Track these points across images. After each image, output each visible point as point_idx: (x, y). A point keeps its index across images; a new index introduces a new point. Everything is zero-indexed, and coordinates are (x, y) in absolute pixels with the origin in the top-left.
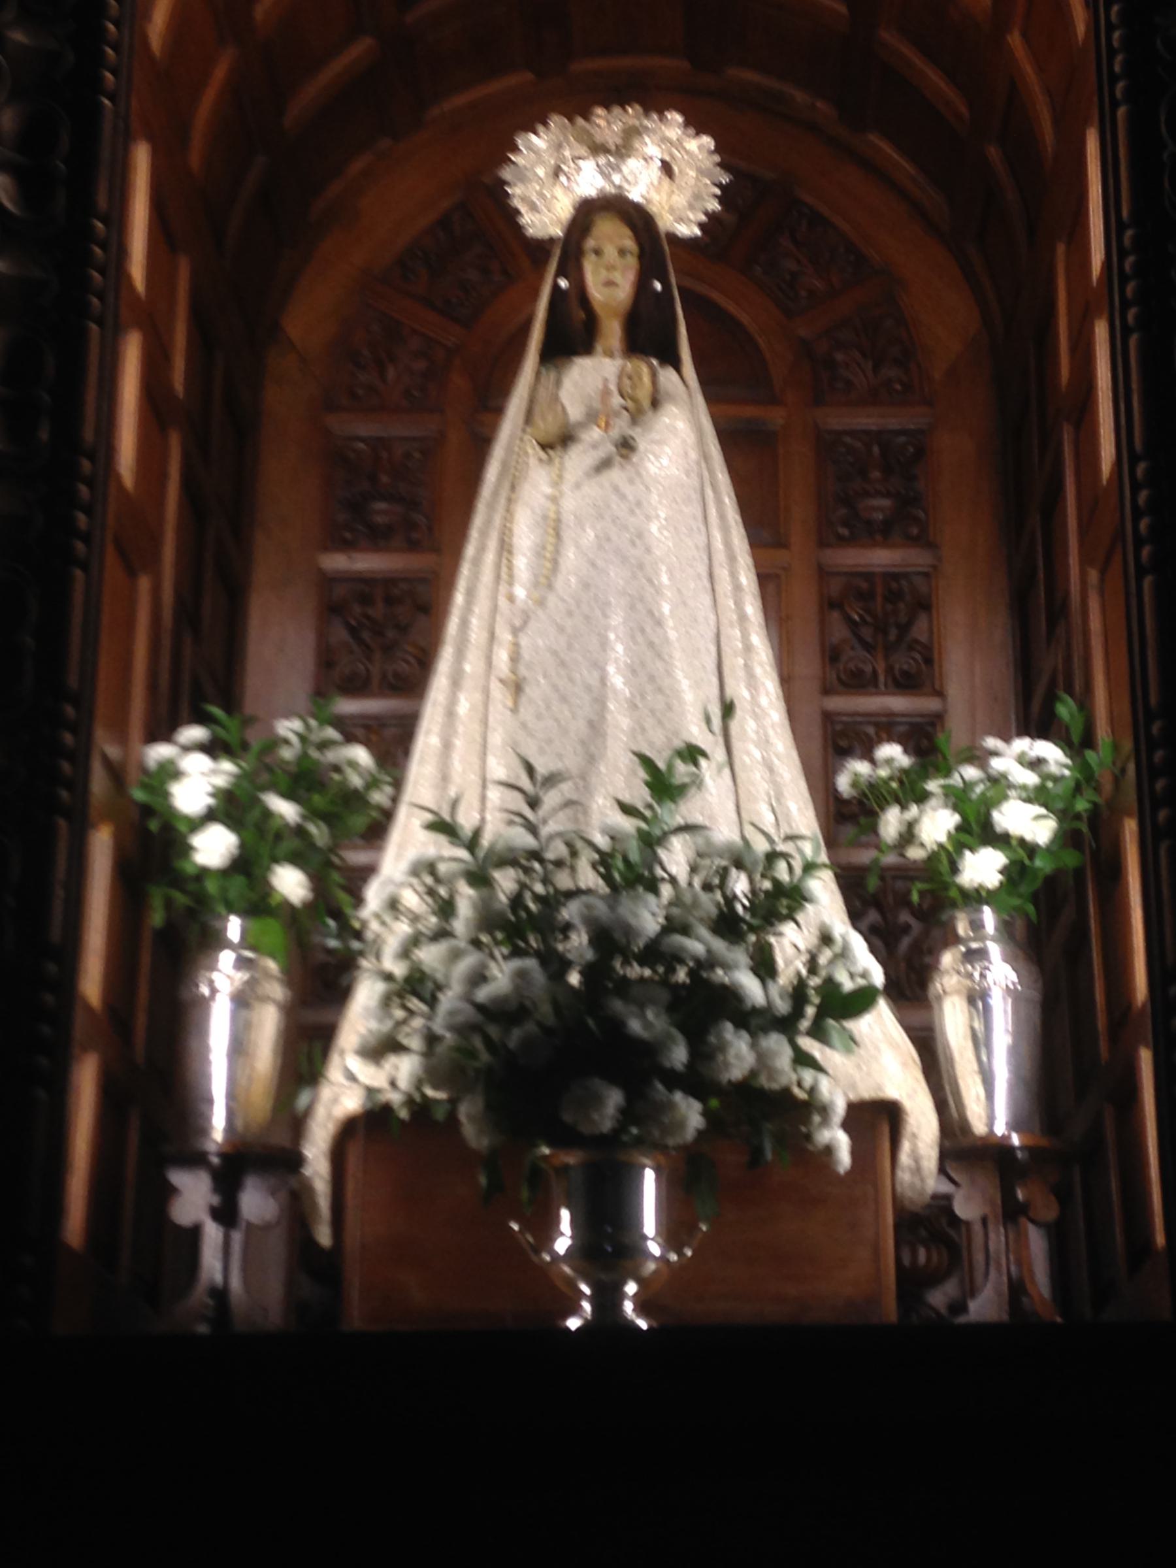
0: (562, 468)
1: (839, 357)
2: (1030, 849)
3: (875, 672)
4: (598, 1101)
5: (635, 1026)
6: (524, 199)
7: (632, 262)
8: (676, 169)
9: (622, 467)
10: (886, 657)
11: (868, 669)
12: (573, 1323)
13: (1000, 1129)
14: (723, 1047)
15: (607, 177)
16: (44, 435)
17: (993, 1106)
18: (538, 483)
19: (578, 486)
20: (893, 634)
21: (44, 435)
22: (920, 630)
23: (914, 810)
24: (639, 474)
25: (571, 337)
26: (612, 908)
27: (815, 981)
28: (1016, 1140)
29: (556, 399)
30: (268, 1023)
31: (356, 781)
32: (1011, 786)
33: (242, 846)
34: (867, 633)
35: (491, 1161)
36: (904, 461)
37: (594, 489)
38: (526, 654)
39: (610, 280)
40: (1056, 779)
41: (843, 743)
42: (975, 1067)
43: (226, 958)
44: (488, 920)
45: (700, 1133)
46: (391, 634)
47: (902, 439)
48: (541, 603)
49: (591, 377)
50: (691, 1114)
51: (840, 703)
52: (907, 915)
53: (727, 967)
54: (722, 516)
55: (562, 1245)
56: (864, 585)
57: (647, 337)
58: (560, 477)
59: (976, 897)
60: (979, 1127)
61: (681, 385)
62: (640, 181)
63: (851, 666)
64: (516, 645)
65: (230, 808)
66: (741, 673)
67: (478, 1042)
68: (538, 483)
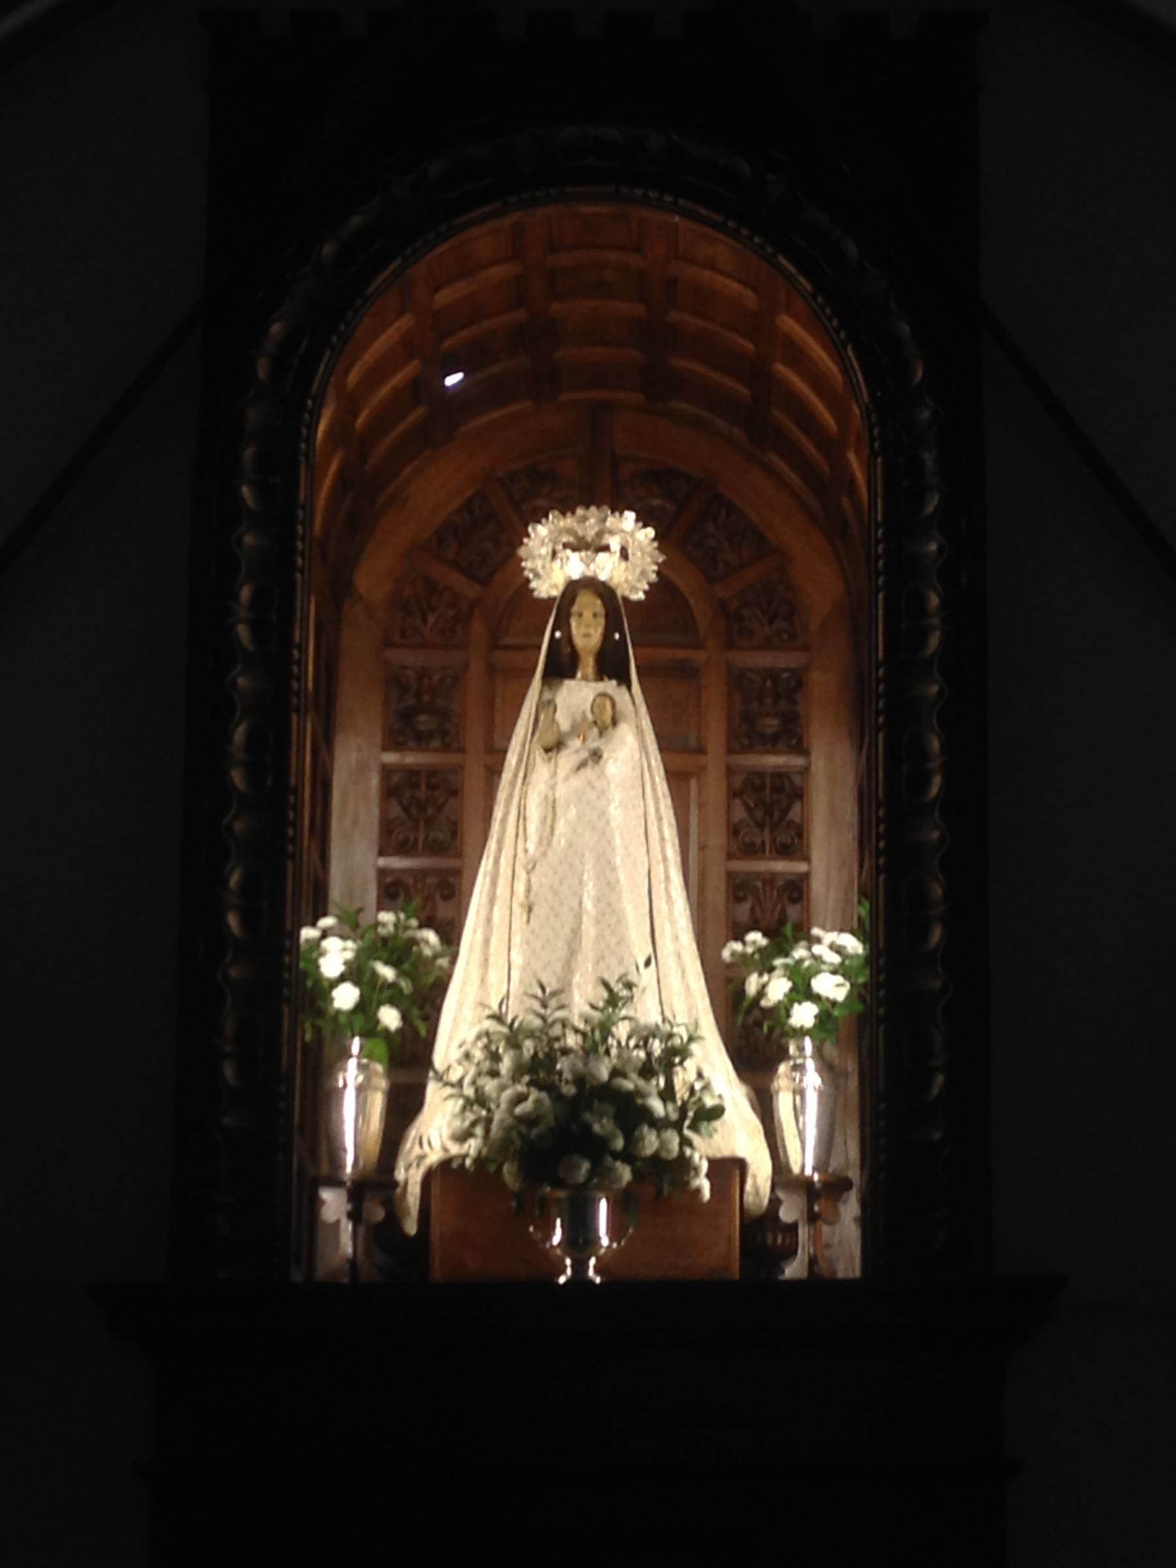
0: (556, 766)
1: (746, 613)
2: (834, 1003)
3: (763, 843)
4: (578, 1167)
5: (596, 1128)
6: (534, 571)
7: (602, 621)
8: (630, 552)
9: (593, 768)
10: (772, 831)
11: (759, 841)
12: (562, 1280)
13: (808, 1172)
14: (642, 1138)
15: (588, 565)
16: (269, 782)
17: (803, 1157)
18: (542, 772)
19: (566, 779)
20: (777, 814)
21: (269, 782)
22: (795, 813)
23: (766, 977)
24: (603, 772)
25: (562, 666)
26: (586, 1064)
27: (693, 1099)
28: (816, 1177)
29: (553, 720)
30: (377, 1102)
31: (427, 952)
32: (823, 962)
33: (362, 995)
34: (759, 814)
35: (519, 1195)
36: (788, 690)
37: (577, 782)
38: (535, 887)
39: (587, 632)
40: (851, 957)
41: (741, 894)
42: (796, 1132)
43: (352, 1064)
44: (518, 1071)
45: (629, 1183)
46: (430, 811)
47: (786, 675)
48: (544, 854)
49: (578, 695)
50: (625, 1173)
51: (739, 866)
52: (756, 1046)
53: (644, 1095)
54: (654, 789)
55: (557, 1239)
56: (757, 782)
57: (610, 665)
58: (555, 774)
59: (800, 1033)
60: (796, 1169)
61: (631, 701)
62: (607, 568)
63: (747, 839)
64: (529, 881)
65: (355, 973)
66: (663, 894)
67: (514, 1135)
68: (542, 772)
